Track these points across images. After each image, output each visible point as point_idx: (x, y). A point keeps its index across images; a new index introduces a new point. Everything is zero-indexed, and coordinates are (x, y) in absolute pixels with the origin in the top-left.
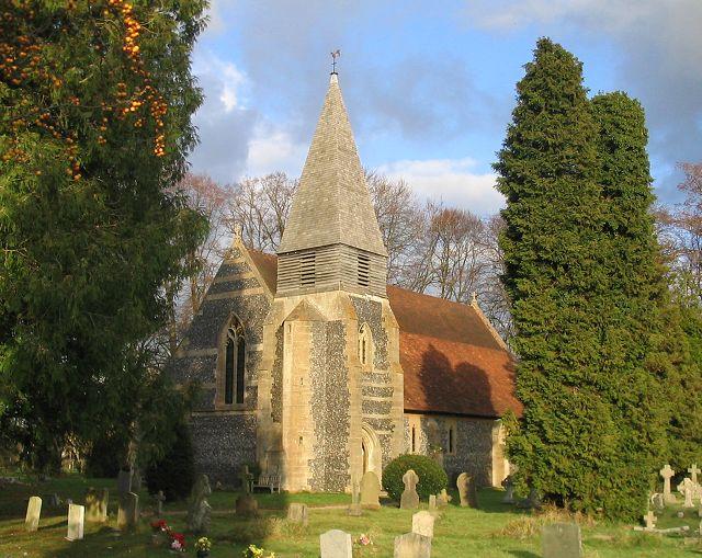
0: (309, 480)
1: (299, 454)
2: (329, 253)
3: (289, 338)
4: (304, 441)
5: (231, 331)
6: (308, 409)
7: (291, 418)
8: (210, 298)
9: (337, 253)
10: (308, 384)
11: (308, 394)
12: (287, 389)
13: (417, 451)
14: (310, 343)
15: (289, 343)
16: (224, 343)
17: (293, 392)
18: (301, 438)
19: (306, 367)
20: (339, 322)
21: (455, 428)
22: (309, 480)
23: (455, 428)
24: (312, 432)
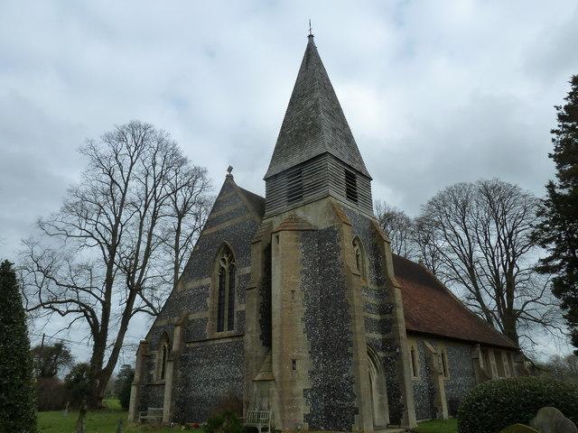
0: (306, 416)
1: (293, 382)
2: (316, 165)
3: (277, 250)
4: (298, 366)
5: (224, 260)
6: (301, 326)
7: (281, 338)
8: (205, 233)
9: (324, 162)
10: (299, 297)
11: (300, 310)
12: (276, 306)
13: (508, 376)
14: (300, 254)
15: (276, 255)
16: (217, 272)
17: (282, 309)
18: (294, 362)
19: (297, 280)
20: (330, 230)
21: (445, 352)
22: (306, 416)
23: (445, 352)
24: (306, 355)
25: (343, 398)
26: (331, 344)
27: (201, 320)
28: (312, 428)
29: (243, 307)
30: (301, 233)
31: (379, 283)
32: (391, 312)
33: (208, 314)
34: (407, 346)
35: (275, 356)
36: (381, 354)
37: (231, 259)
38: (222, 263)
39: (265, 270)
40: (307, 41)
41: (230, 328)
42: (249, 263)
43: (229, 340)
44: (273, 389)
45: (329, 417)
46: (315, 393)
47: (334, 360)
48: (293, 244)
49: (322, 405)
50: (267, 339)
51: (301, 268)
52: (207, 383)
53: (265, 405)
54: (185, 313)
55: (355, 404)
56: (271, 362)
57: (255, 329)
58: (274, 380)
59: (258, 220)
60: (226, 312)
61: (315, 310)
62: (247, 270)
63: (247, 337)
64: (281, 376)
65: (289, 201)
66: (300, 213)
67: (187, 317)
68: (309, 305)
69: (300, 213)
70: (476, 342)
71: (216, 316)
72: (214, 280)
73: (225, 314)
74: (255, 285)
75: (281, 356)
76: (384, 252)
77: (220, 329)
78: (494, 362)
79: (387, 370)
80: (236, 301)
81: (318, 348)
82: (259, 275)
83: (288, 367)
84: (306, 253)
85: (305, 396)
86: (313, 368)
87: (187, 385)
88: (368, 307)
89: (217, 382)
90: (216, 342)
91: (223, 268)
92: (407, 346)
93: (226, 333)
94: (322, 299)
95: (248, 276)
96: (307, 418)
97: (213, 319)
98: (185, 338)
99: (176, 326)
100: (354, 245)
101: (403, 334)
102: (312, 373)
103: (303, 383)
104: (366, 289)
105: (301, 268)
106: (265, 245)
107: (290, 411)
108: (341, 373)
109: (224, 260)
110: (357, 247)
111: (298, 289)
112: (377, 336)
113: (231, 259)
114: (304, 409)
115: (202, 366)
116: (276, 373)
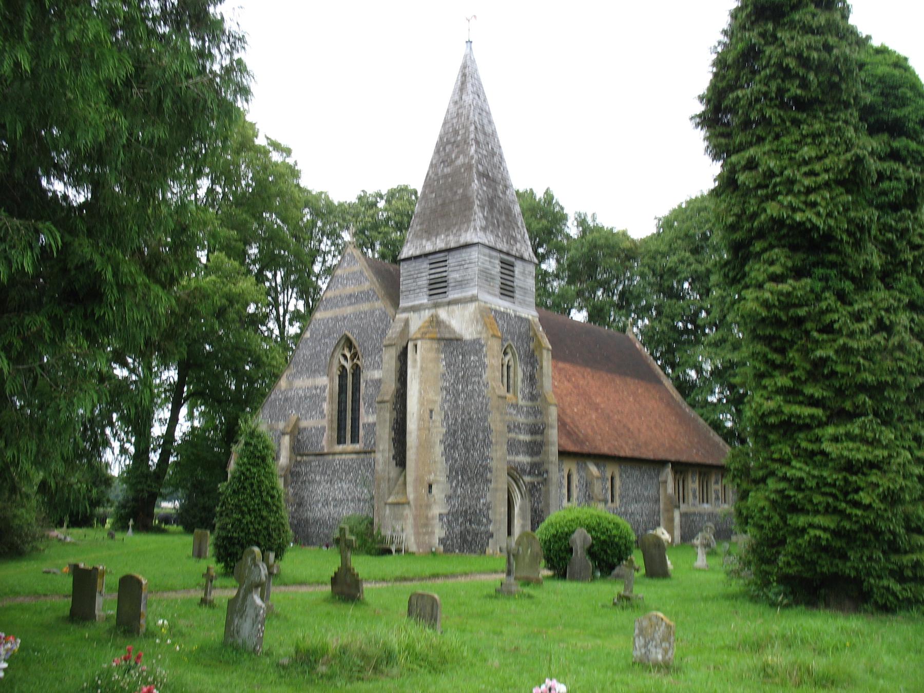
1: (428, 506)
5: (345, 356)
6: (439, 449)
10: (438, 417)
11: (439, 430)
12: (412, 425)
16: (336, 372)
18: (430, 486)
19: (436, 398)
20: (476, 341)
24: (442, 478)
25: (479, 523)
26: (467, 471)
27: (317, 429)
28: (446, 550)
29: (371, 419)
30: (442, 343)
31: (533, 398)
32: (542, 433)
33: (325, 423)
34: (557, 471)
35: (410, 479)
36: (527, 479)
37: (355, 356)
38: (343, 362)
39: (399, 379)
40: (463, 49)
41: (355, 439)
42: (378, 366)
43: (354, 456)
44: (408, 512)
45: (464, 541)
46: (450, 519)
47: (472, 486)
48: (432, 355)
49: (457, 529)
50: (400, 459)
51: (442, 384)
52: (326, 503)
53: (398, 528)
54: (293, 418)
55: (491, 528)
56: (405, 483)
57: (387, 447)
58: (408, 503)
59: (390, 311)
60: (349, 422)
61: (455, 432)
62: (377, 374)
63: (379, 456)
64: (416, 499)
65: (431, 295)
66: (443, 314)
67: (296, 425)
68: (449, 427)
69: (443, 314)
70: (662, 463)
71: (335, 425)
72: (332, 380)
73: (346, 424)
74: (387, 398)
75: (418, 480)
76: (541, 361)
77: (341, 440)
78: (696, 485)
79: (532, 495)
80: (362, 411)
81: (457, 473)
82: (390, 387)
83: (424, 491)
84: (448, 365)
85: (441, 519)
86: (450, 492)
87: (300, 505)
88: (512, 427)
89: (338, 503)
90: (337, 457)
91: (343, 367)
92: (557, 471)
93: (349, 447)
94: (463, 420)
95: (378, 383)
96: (442, 541)
97: (331, 428)
98: (297, 449)
99: (283, 434)
100: (505, 353)
101: (554, 457)
102: (449, 498)
103: (439, 509)
104: (515, 406)
105: (442, 384)
106: (400, 349)
107: (425, 534)
108: (478, 499)
109: (345, 356)
110: (509, 356)
111: (437, 408)
112: (524, 459)
113: (355, 356)
114: (439, 532)
115: (320, 483)
116: (411, 496)
